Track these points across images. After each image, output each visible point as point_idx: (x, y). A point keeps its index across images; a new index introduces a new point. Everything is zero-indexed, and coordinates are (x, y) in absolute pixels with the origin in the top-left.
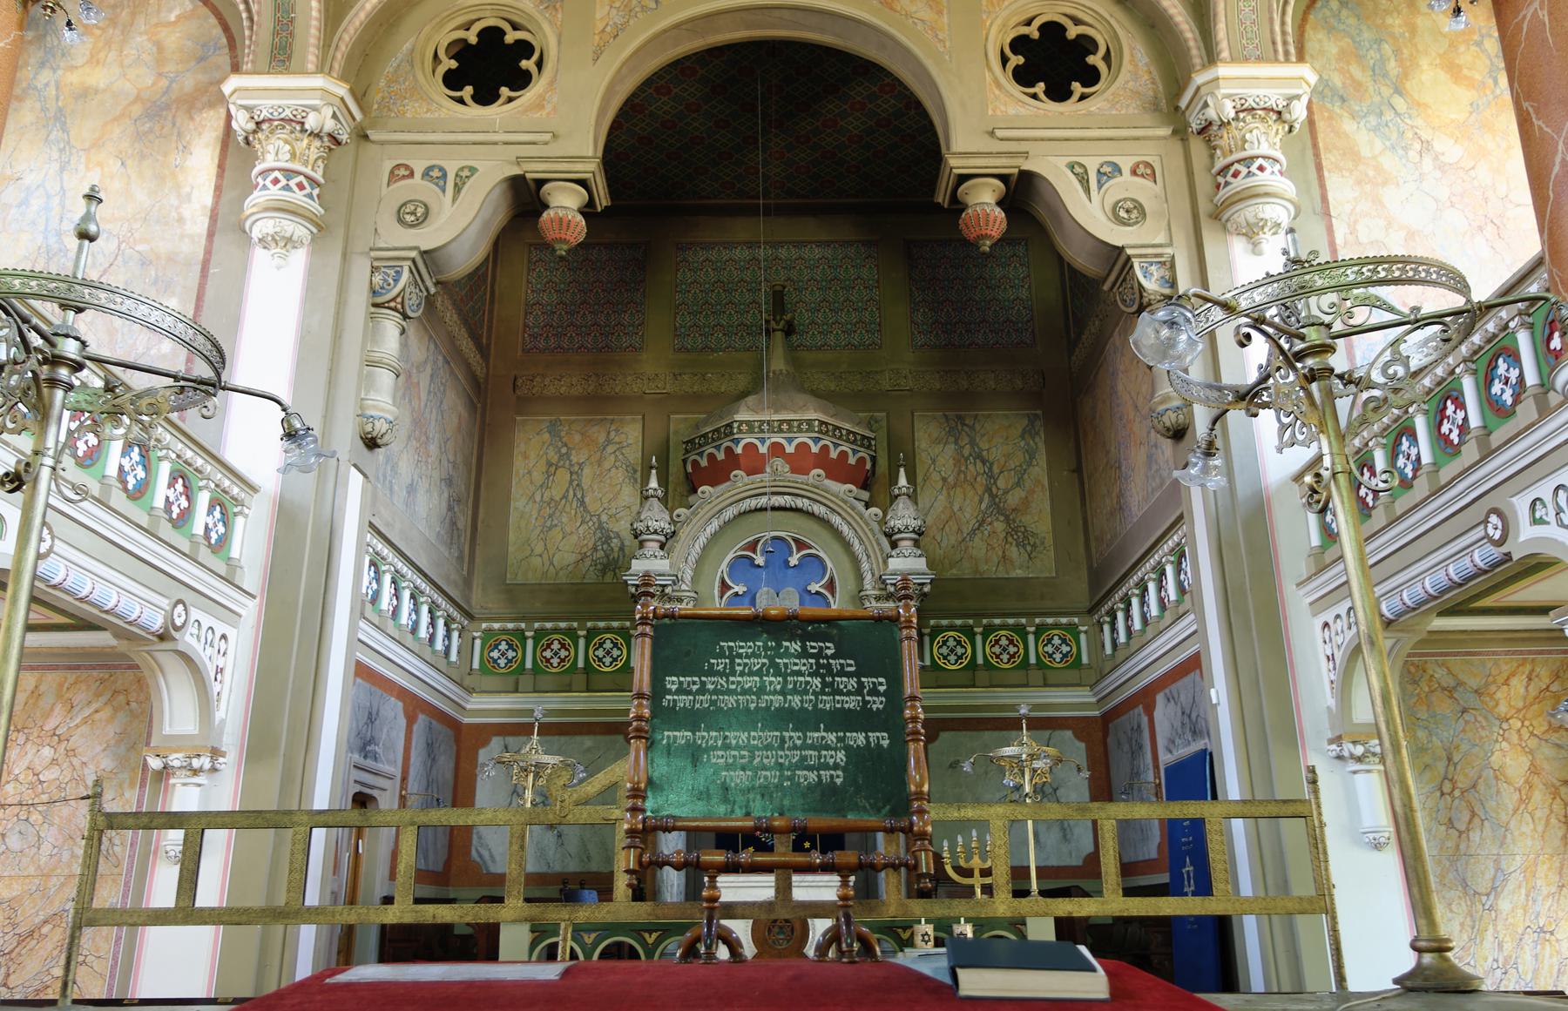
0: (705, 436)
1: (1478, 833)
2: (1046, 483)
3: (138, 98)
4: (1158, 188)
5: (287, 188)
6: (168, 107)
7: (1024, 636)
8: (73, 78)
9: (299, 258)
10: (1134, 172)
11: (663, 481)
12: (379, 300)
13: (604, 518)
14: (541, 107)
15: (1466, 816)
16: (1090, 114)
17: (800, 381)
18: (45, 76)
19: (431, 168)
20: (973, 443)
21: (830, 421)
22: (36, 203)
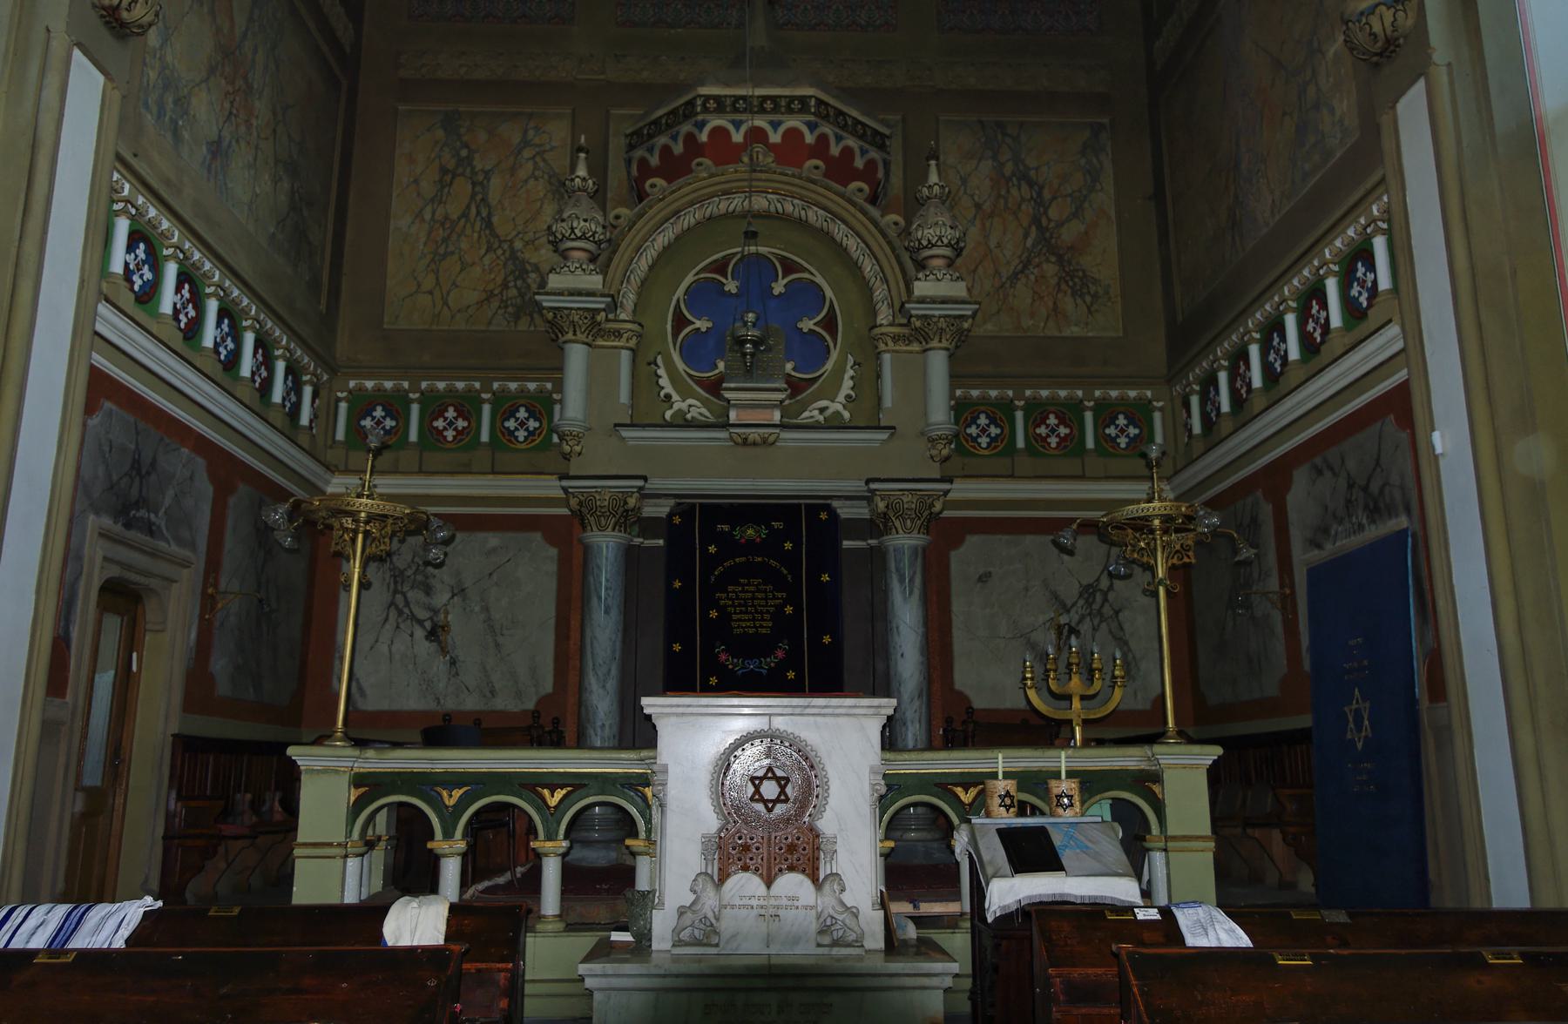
0: (656, 122)
2: (1112, 213)
11: (599, 170)
13: (518, 245)
21: (831, 101)
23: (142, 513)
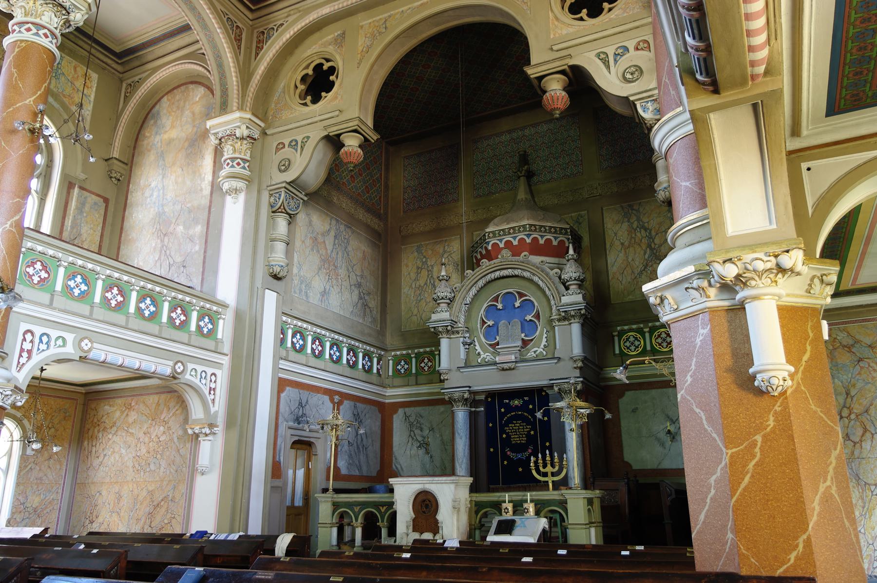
1: (869, 443)
3: (187, 139)
4: (651, 55)
5: (233, 166)
6: (196, 140)
7: (643, 334)
8: (166, 136)
9: (242, 197)
10: (637, 49)
12: (274, 209)
14: (336, 98)
15: (860, 431)
16: (611, 20)
17: (534, 205)
18: (158, 138)
19: (291, 142)
20: (638, 220)
22: (155, 194)
23: (305, 418)
